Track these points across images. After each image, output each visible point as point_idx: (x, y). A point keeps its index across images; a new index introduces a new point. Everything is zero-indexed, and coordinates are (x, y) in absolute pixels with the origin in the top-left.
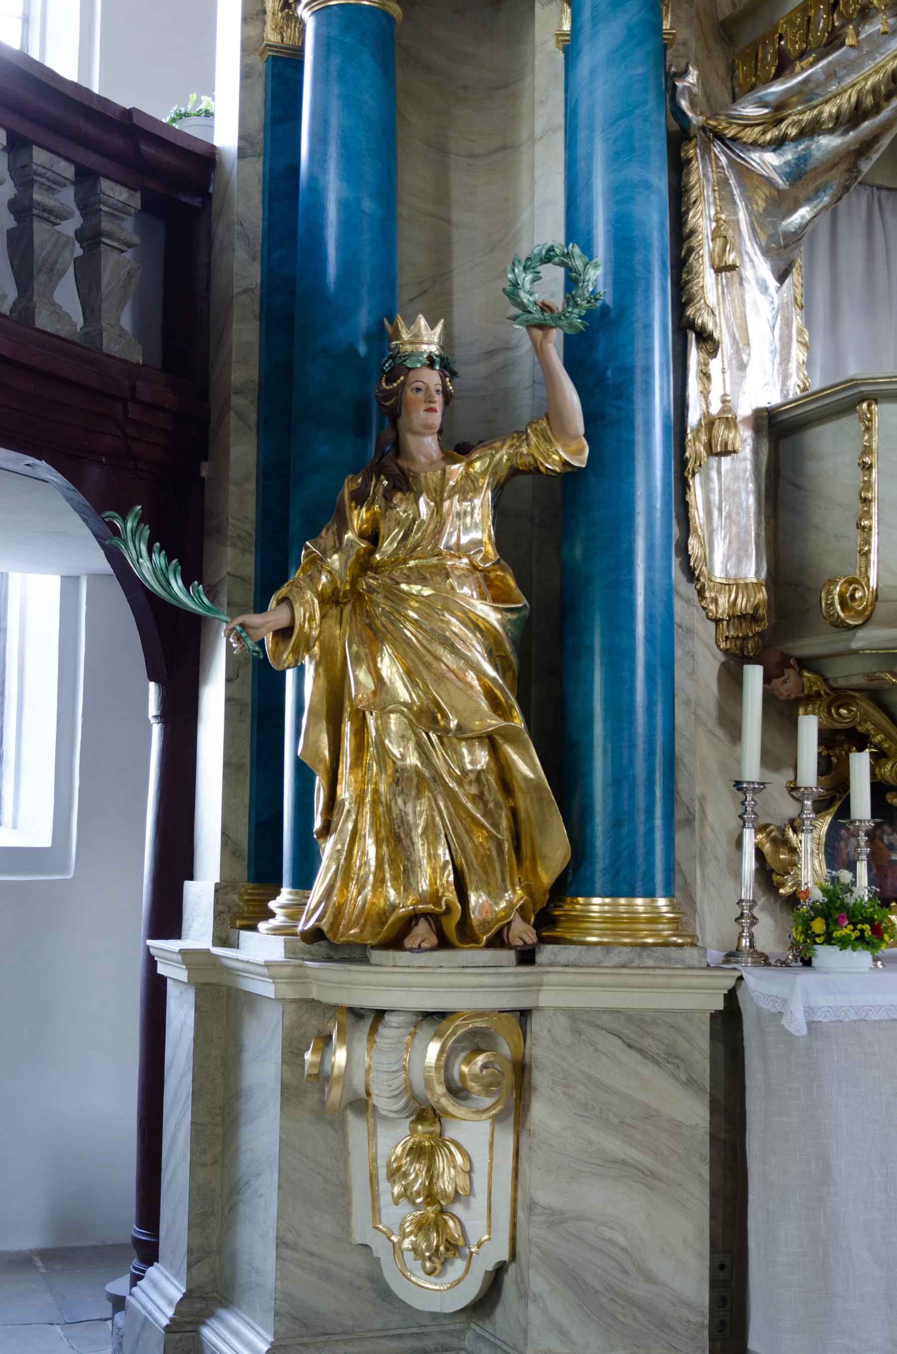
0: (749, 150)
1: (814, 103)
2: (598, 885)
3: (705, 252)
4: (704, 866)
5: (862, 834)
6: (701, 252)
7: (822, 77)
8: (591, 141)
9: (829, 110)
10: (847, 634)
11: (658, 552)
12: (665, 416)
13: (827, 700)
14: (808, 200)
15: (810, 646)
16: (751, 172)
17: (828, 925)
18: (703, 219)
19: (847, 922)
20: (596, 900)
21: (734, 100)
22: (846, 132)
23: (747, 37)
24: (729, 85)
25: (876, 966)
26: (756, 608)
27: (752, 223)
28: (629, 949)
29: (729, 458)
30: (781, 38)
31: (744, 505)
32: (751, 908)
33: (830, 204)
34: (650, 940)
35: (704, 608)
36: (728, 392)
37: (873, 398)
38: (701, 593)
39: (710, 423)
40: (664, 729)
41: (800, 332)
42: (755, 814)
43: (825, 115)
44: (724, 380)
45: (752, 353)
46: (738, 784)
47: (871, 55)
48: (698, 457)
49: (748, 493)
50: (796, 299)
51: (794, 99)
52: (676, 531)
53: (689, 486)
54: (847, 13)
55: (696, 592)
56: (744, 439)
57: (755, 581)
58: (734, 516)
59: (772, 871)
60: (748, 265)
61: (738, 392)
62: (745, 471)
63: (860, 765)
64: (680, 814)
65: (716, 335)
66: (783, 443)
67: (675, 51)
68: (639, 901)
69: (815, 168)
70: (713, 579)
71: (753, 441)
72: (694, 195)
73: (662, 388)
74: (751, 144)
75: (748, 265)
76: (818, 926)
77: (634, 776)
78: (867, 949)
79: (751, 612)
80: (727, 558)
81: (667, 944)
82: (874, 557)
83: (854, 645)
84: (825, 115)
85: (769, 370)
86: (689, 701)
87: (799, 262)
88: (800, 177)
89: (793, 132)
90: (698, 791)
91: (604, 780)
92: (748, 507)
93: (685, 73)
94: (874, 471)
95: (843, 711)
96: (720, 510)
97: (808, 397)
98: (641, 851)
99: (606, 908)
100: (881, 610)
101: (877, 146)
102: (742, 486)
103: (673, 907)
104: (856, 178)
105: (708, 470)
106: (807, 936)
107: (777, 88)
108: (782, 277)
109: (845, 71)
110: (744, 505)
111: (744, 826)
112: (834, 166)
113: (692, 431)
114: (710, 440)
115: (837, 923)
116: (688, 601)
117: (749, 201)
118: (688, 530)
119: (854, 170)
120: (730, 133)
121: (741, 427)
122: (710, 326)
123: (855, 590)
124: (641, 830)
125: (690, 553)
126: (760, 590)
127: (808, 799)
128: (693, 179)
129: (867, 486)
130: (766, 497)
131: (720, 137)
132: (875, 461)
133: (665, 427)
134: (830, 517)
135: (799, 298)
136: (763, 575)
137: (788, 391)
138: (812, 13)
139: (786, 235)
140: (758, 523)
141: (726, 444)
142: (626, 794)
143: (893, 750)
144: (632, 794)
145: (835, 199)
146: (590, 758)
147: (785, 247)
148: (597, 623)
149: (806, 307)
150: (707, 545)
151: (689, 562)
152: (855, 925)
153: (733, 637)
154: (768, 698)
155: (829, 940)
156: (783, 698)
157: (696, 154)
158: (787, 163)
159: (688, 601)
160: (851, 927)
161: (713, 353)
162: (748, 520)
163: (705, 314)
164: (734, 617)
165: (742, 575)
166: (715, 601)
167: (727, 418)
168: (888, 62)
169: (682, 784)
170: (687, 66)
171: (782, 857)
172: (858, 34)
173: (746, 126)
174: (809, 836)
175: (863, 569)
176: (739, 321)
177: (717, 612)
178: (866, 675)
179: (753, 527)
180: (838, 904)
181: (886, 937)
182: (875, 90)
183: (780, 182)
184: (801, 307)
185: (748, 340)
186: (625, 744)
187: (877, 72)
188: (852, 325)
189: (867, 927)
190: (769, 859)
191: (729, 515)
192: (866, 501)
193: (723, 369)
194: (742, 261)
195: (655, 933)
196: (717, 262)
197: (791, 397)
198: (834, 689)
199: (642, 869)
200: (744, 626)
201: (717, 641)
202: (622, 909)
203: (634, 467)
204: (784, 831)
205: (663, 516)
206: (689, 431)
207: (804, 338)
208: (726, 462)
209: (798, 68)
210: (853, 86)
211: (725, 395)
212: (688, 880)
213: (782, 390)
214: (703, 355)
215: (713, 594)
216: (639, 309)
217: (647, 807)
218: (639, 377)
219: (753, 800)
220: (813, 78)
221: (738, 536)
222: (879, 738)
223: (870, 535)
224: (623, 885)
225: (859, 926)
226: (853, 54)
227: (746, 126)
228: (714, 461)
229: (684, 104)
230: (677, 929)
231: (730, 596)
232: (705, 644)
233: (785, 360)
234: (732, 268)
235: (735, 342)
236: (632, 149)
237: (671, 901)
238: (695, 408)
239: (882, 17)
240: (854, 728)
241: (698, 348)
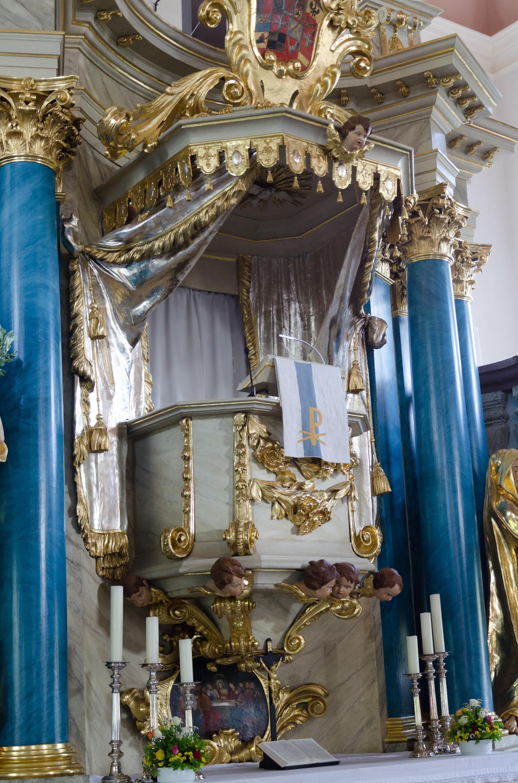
0: (111, 266)
1: (149, 240)
2: (17, 737)
3: (85, 327)
4: (90, 719)
5: (188, 692)
6: (82, 327)
7: (154, 225)
8: (10, 258)
9: (158, 244)
10: (177, 564)
11: (55, 515)
12: (59, 429)
13: (167, 605)
14: (148, 297)
15: (155, 572)
16: (113, 279)
17: (166, 754)
18: (83, 307)
19: (178, 751)
20: (16, 748)
21: (103, 235)
22: (169, 258)
23: (110, 199)
24: (100, 227)
25: (199, 778)
26: (121, 548)
27: (114, 310)
28: (37, 780)
29: (102, 454)
30: (130, 200)
31: (113, 484)
32: (118, 746)
33: (161, 300)
34: (52, 773)
35: (88, 550)
36: (101, 413)
37: (189, 417)
38: (85, 540)
39: (89, 432)
40: (59, 630)
41: (147, 376)
42: (120, 683)
43: (156, 247)
44: (98, 406)
45: (116, 388)
46: (109, 665)
47: (182, 212)
48: (82, 454)
49: (115, 475)
50: (144, 356)
51: (138, 237)
52: (67, 500)
53: (76, 472)
54: (167, 188)
55: (82, 540)
56: (112, 442)
57: (120, 531)
58: (106, 491)
59: (136, 719)
60: (112, 335)
61: (108, 413)
62: (113, 462)
63: (186, 647)
64: (72, 686)
65: (92, 378)
66: (137, 444)
67: (65, 206)
68: (45, 747)
69: (151, 278)
70: (93, 531)
71: (118, 443)
72: (77, 292)
73: (56, 412)
74: (112, 263)
75: (112, 335)
76: (160, 755)
77: (40, 663)
78: (191, 768)
79: (118, 551)
80: (102, 517)
81: (62, 775)
82: (192, 514)
83: (181, 570)
84: (156, 247)
85: (127, 399)
86: (79, 610)
87: (145, 333)
88: (142, 283)
89: (137, 256)
90: (85, 670)
91: (21, 666)
92: (115, 485)
93: (70, 219)
94: (191, 461)
95: (177, 612)
96: (97, 487)
97: (153, 415)
98: (45, 713)
99: (22, 753)
100: (197, 547)
101: (188, 266)
102: (111, 471)
103: (67, 749)
104: (176, 284)
105: (89, 462)
106: (153, 762)
107: (127, 230)
108: (133, 343)
109: (167, 222)
110: (113, 484)
111: (113, 692)
112: (162, 277)
113: (78, 438)
114: (90, 443)
115: (172, 752)
116: (77, 546)
117: (112, 297)
118: (77, 500)
119: (174, 280)
120: (99, 256)
121: (109, 435)
122: (89, 373)
123: (181, 535)
124: (45, 698)
125: (78, 514)
126: (124, 537)
127: (153, 671)
128: (77, 282)
129: (187, 470)
130: (126, 476)
131: (93, 258)
132: (191, 455)
133: (58, 435)
134: (166, 490)
135: (146, 355)
136: (125, 527)
137: (140, 412)
138: (147, 187)
139: (135, 317)
140: (122, 495)
141: (100, 445)
142: (34, 675)
143: (210, 636)
144: (39, 674)
145: (164, 297)
146: (11, 652)
147: (135, 324)
148: (15, 563)
149: (150, 360)
150: (89, 509)
151: (77, 520)
152: (183, 753)
153: (107, 568)
154: (128, 607)
155: (167, 764)
156: (139, 606)
157: (78, 268)
158: (134, 275)
159: (77, 546)
160: (180, 754)
161: (91, 389)
162: (116, 493)
163: (85, 365)
164: (107, 555)
165: (112, 528)
166: (95, 545)
167: (101, 429)
168: (192, 217)
169: (75, 666)
170: (72, 215)
171: (141, 709)
172: (174, 200)
173: (109, 252)
174: (155, 696)
175: (186, 522)
176: (107, 369)
177: (96, 552)
178: (189, 589)
179: (118, 497)
180: (172, 740)
181: (203, 759)
182: (184, 234)
183: (131, 286)
184: (148, 361)
185: (114, 381)
186: (34, 642)
187: (185, 223)
188: (179, 372)
189: (191, 753)
190: (133, 712)
191: (103, 490)
192: (186, 480)
193: (98, 398)
194: (109, 333)
195: (55, 768)
196: (92, 333)
197: (142, 415)
198: (171, 599)
199: (46, 724)
200: (114, 560)
201: (97, 570)
202: (33, 753)
203: (38, 461)
204: (143, 692)
205: (57, 492)
206: (76, 437)
207: (149, 379)
208: (101, 457)
209: (139, 220)
210: (172, 230)
211: (99, 415)
212: (80, 730)
213: (136, 411)
214: (85, 390)
215: (93, 541)
216: (41, 362)
217: (48, 683)
218: (41, 404)
219: (118, 674)
220: (148, 225)
221: (109, 503)
222: (201, 628)
223: (189, 501)
224: (32, 738)
225: (186, 753)
226: (171, 212)
227: (109, 252)
228: (93, 456)
229: (70, 238)
230: (71, 764)
231: (104, 541)
232: (89, 573)
233: (138, 393)
234: (102, 337)
235: (105, 382)
236: (36, 264)
237: (66, 745)
238: (80, 424)
239: (187, 191)
240: (185, 622)
241: (81, 386)
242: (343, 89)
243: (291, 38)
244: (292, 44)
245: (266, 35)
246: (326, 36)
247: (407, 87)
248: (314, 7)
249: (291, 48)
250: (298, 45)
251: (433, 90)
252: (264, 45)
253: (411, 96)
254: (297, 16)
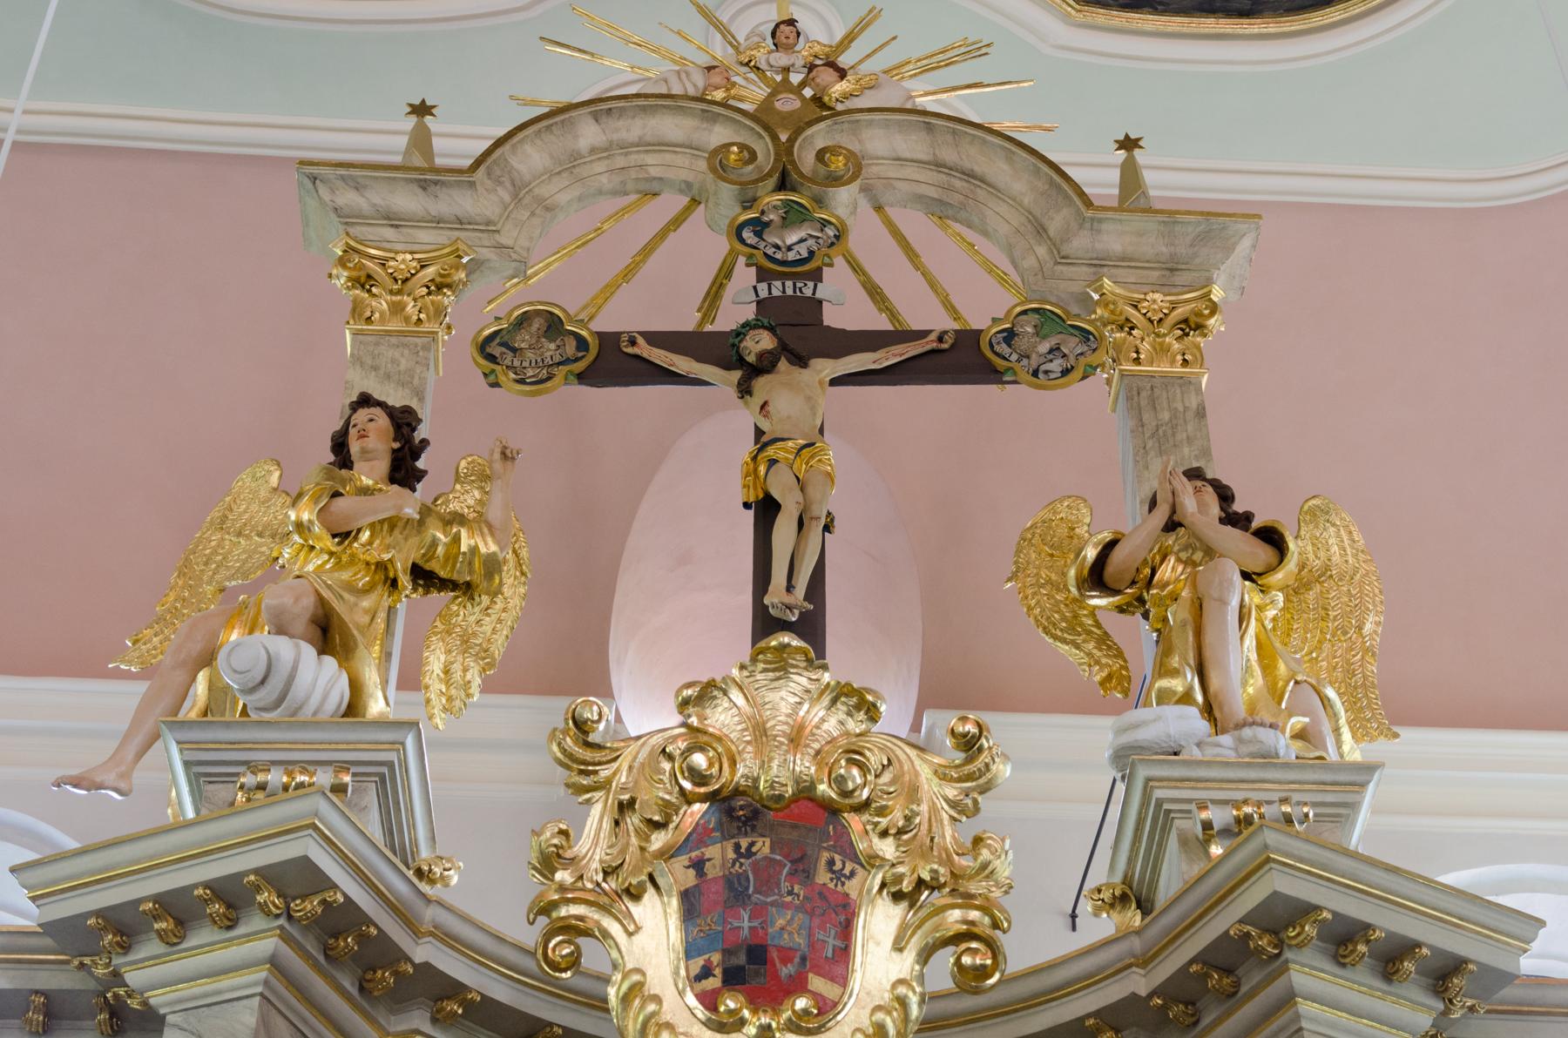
242: (1089, 1016)
243: (780, 949)
244: (786, 960)
245: (716, 958)
246: (879, 922)
247: (1228, 971)
248: (838, 866)
249: (786, 971)
250: (804, 959)
251: (1277, 963)
252: (713, 983)
253: (1244, 989)
254: (789, 899)
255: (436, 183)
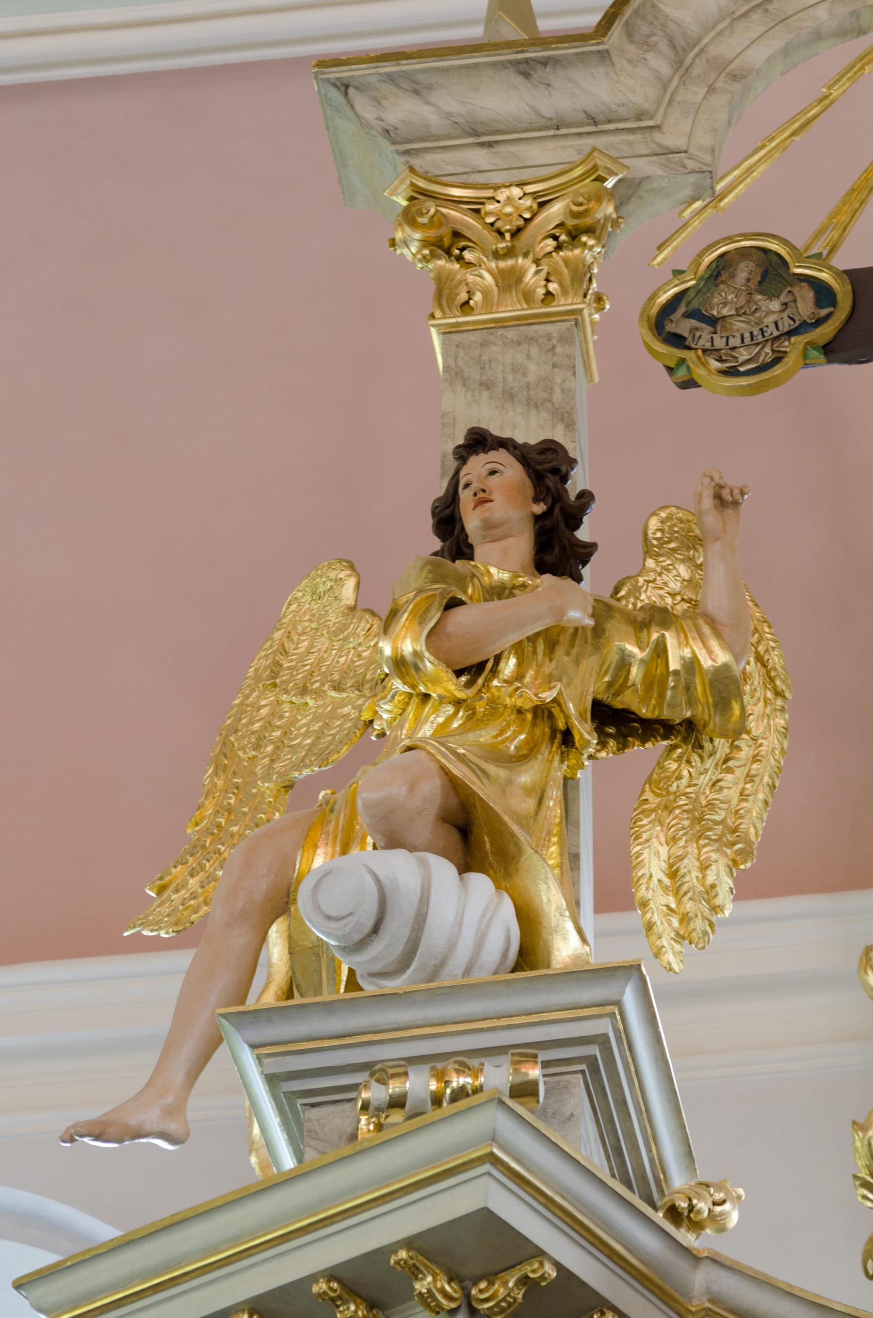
255: (544, 63)
